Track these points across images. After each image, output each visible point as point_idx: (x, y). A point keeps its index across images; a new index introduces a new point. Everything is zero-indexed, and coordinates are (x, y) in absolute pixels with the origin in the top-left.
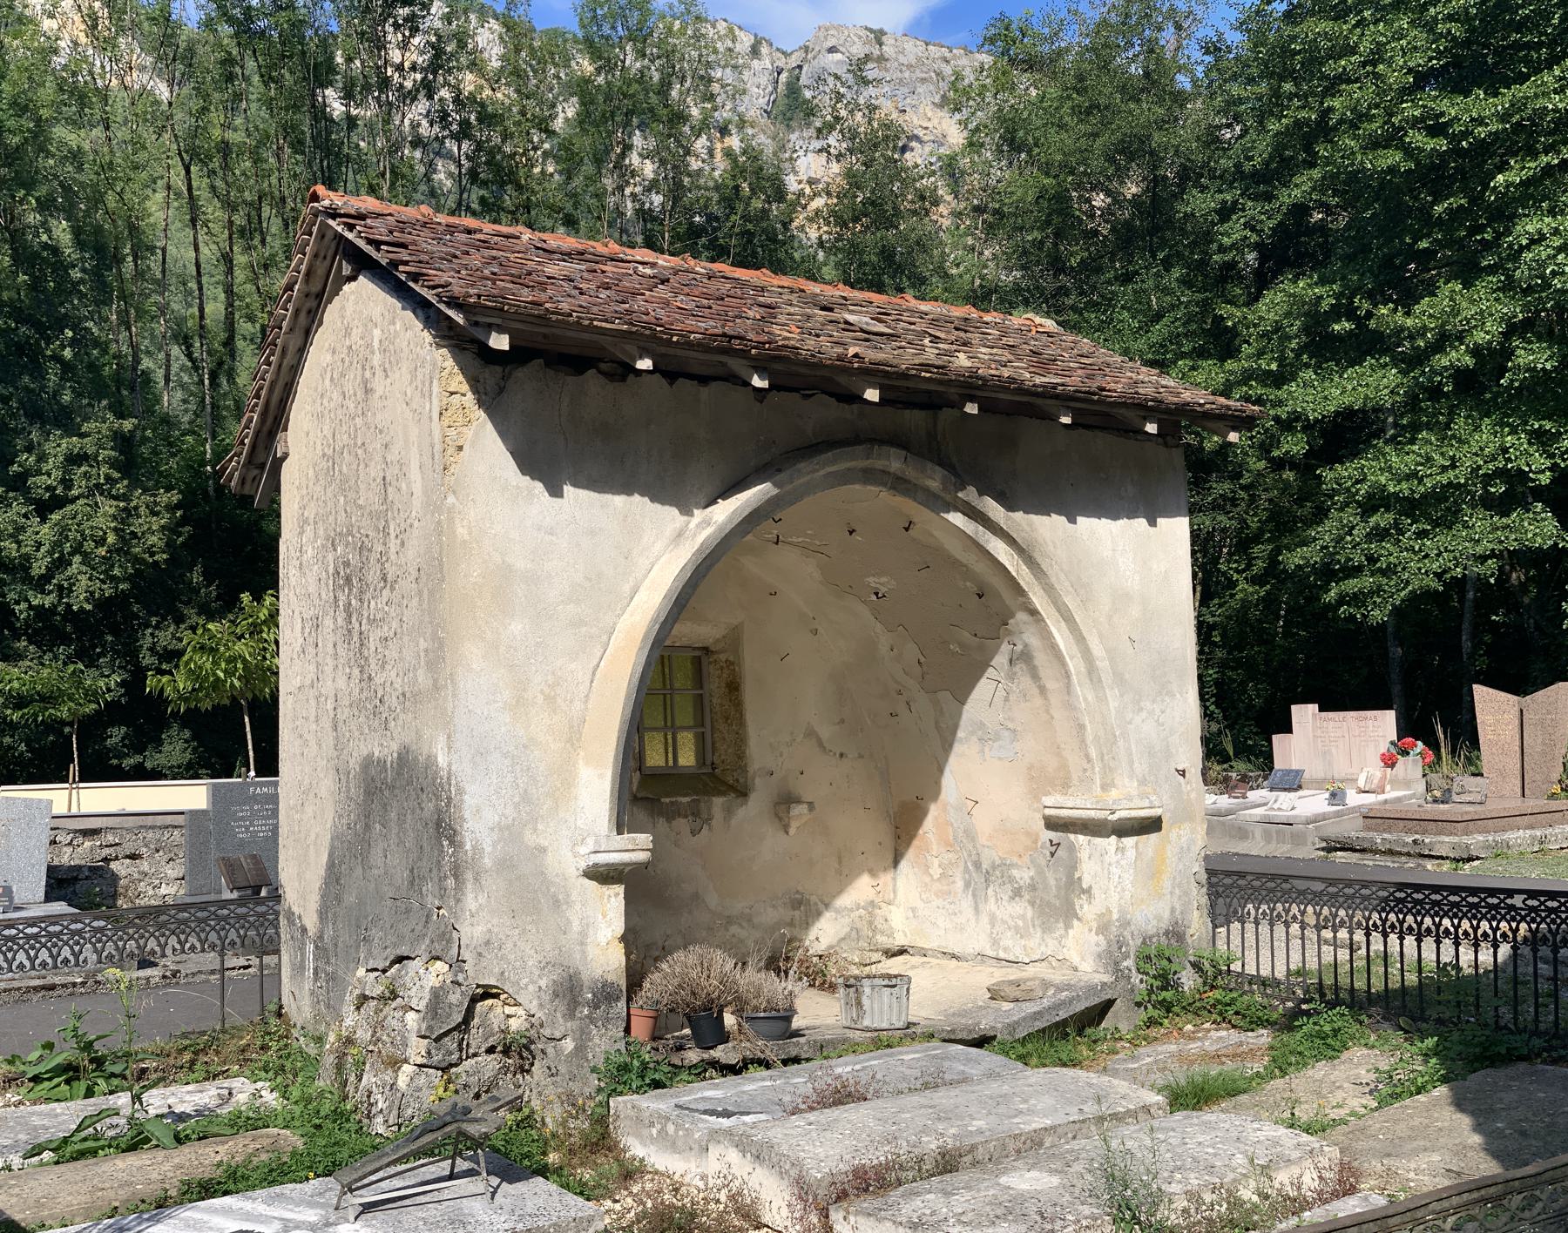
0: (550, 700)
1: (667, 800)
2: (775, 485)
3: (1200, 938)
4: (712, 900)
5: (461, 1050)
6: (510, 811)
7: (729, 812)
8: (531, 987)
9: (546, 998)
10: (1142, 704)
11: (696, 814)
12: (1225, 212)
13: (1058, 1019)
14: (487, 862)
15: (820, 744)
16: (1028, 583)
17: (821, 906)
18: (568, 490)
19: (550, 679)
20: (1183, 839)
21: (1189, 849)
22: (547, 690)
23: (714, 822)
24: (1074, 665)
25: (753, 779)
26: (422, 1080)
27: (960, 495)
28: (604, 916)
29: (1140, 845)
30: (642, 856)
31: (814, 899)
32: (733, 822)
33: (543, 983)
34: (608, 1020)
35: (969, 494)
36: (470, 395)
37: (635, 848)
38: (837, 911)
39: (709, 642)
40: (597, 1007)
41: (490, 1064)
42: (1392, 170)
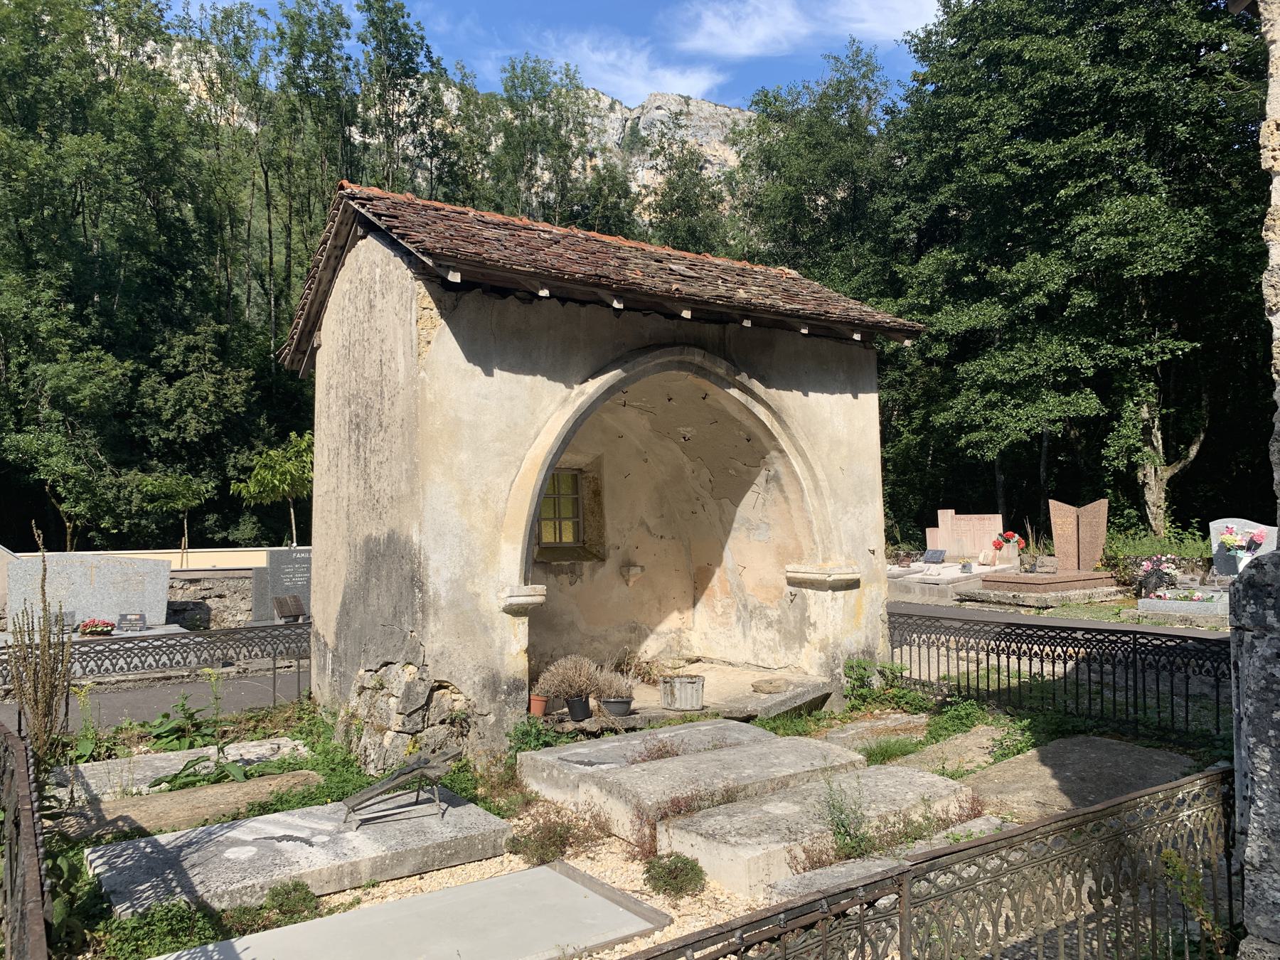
0: (484, 501)
4: (582, 626)
6: (458, 571)
7: (593, 571)
8: (469, 682)
9: (478, 688)
12: (898, 209)
14: (443, 603)
15: (649, 531)
17: (648, 631)
18: (496, 372)
19: (484, 489)
22: (482, 496)
24: (806, 484)
26: (399, 741)
28: (515, 637)
31: (644, 626)
32: (596, 577)
33: (476, 679)
35: (743, 377)
37: (535, 594)
40: (510, 694)
41: (442, 731)
42: (999, 185)
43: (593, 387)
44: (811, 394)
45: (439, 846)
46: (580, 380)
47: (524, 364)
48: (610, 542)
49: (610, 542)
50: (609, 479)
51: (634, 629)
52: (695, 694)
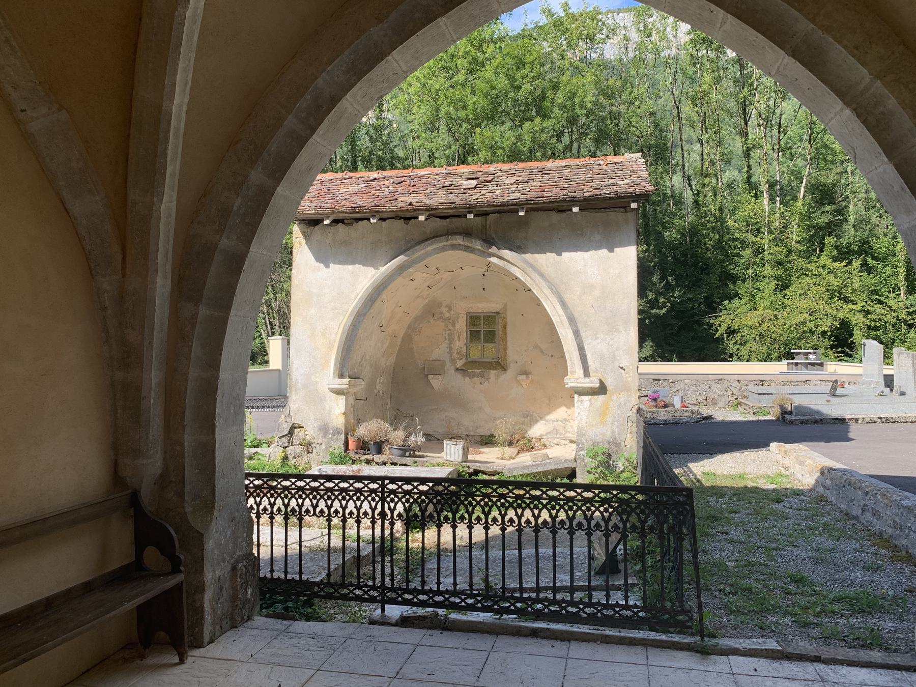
0: (323, 334)
2: (406, 256)
3: (631, 448)
5: (289, 443)
7: (498, 376)
8: (311, 426)
9: (316, 430)
10: (598, 336)
11: (483, 376)
14: (300, 385)
18: (332, 265)
20: (621, 400)
21: (625, 404)
23: (490, 380)
25: (510, 364)
26: (276, 450)
27: (490, 250)
28: (338, 405)
29: (592, 400)
30: (345, 386)
31: (534, 414)
33: (315, 425)
35: (494, 249)
36: (302, 237)
37: (344, 384)
38: (547, 421)
39: (498, 310)
40: (334, 435)
41: (299, 449)
43: (385, 269)
46: (383, 264)
47: (349, 259)
50: (511, 319)
52: (456, 452)
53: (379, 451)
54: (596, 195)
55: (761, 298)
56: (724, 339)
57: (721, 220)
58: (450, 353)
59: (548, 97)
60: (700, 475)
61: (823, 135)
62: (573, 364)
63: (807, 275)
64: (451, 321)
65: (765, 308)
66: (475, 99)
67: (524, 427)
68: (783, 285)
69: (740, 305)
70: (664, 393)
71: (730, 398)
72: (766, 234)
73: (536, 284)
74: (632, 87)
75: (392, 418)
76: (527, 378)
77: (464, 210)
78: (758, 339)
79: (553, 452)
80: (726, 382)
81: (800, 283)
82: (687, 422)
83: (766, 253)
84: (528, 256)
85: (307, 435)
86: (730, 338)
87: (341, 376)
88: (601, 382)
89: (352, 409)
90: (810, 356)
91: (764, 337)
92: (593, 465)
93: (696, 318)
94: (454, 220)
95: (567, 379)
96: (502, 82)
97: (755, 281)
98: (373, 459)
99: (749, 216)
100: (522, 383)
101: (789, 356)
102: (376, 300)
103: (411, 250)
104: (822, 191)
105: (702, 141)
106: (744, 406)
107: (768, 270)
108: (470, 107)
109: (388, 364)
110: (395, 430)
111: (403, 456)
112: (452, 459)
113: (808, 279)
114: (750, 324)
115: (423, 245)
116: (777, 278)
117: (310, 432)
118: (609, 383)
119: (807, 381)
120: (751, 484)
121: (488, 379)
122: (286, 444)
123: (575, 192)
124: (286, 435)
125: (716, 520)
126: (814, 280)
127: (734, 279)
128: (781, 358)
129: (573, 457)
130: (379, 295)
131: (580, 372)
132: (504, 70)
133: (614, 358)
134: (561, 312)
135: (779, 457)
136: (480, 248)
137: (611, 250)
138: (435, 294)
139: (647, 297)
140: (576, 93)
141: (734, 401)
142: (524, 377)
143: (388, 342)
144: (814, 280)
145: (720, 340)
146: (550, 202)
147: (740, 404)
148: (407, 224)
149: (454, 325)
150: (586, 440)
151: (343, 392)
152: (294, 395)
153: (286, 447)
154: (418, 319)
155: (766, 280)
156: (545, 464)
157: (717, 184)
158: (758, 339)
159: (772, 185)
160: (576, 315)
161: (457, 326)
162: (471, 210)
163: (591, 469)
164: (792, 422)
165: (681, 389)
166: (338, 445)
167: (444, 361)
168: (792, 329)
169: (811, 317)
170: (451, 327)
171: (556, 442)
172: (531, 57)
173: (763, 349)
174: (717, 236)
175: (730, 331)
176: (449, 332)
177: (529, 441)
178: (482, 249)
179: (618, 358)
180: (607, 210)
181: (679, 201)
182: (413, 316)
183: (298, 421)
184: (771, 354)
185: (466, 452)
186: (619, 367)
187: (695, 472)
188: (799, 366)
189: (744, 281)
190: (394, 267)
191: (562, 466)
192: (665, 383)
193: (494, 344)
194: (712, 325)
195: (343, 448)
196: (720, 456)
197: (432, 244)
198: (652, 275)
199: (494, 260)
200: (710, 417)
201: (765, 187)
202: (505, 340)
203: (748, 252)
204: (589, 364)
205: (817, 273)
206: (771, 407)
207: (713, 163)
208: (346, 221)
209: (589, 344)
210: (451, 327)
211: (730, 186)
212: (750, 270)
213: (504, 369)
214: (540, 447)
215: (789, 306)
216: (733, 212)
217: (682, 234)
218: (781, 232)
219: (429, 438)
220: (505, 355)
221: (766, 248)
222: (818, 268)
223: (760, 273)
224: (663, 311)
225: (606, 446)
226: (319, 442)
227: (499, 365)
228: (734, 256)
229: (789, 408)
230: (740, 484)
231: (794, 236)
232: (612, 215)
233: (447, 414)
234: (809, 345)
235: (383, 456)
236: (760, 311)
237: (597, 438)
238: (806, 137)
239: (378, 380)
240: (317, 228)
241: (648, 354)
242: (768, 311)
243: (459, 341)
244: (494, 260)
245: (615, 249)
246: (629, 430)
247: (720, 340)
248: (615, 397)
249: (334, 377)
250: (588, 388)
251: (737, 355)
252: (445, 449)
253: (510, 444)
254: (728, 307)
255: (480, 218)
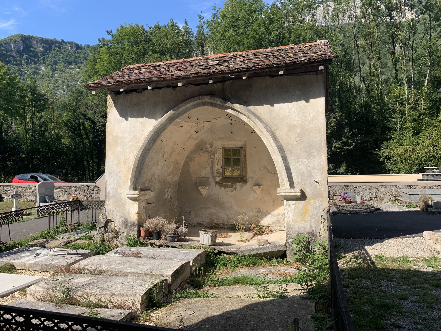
0: (125, 163)
1: (225, 183)
2: (173, 110)
3: (324, 237)
4: (236, 208)
5: (105, 231)
6: (115, 185)
7: (241, 187)
8: (118, 221)
9: (121, 223)
10: (299, 160)
11: (232, 187)
13: (260, 252)
14: (111, 195)
15: (268, 171)
16: (253, 126)
17: (267, 213)
18: (129, 119)
19: (125, 158)
20: (316, 204)
21: (319, 207)
22: (124, 160)
23: (237, 189)
26: (98, 236)
27: (226, 105)
28: (133, 208)
30: (137, 196)
31: (264, 211)
32: (242, 189)
33: (120, 220)
34: (134, 230)
35: (229, 104)
36: (112, 102)
37: (136, 194)
38: (272, 215)
39: (242, 145)
40: (131, 227)
44: (275, 105)
45: (45, 265)
48: (249, 176)
49: (249, 176)
50: (249, 151)
51: (259, 211)
53: (159, 237)
54: (295, 62)
55: (405, 140)
56: (385, 162)
57: (381, 98)
58: (212, 172)
59: (286, 37)
60: (374, 257)
61: (436, 52)
62: (282, 179)
63: (431, 127)
64: (212, 153)
65: (407, 145)
66: (248, 40)
67: (258, 219)
68: (417, 132)
69: (394, 143)
70: (350, 194)
71: (391, 196)
72: (407, 105)
73: (257, 126)
74: (331, 31)
75: (178, 213)
76: (259, 187)
77: (207, 77)
78: (404, 162)
79: (270, 238)
80: (388, 187)
81: (427, 131)
82: (364, 212)
83: (407, 115)
84: (251, 108)
85: (116, 226)
86: (388, 161)
87: (135, 189)
88: (302, 192)
89: (144, 210)
90: (435, 170)
91: (407, 160)
92: (298, 249)
93: (369, 151)
94: (203, 86)
95: (278, 190)
96: (262, 30)
97: (401, 130)
98: (154, 243)
99: (397, 96)
100: (256, 191)
101: (422, 170)
102: (156, 140)
103: (177, 107)
104: (437, 81)
105: (370, 58)
106: (400, 202)
107: (408, 124)
108: (246, 44)
109: (174, 180)
110: (168, 224)
111: (173, 241)
112: (204, 244)
113: (431, 129)
114: (399, 153)
115: (184, 103)
116: (414, 128)
117: (117, 224)
118: (308, 192)
119: (439, 186)
120: (413, 267)
121: (235, 189)
122: (104, 232)
123: (281, 61)
124: (103, 227)
125: (389, 309)
126: (435, 129)
127: (389, 130)
128: (417, 172)
129: (283, 243)
130: (158, 136)
131: (287, 185)
132: (263, 24)
133: (311, 175)
134: (273, 144)
135: (431, 243)
136: (220, 103)
137: (307, 101)
138: (202, 136)
139: (342, 140)
140: (301, 35)
141: (393, 198)
142: (257, 187)
143: (172, 167)
144: (435, 129)
145: (383, 162)
146: (263, 68)
147: (397, 200)
148: (175, 90)
149: (214, 155)
150: (293, 232)
151: (137, 199)
152: (108, 201)
153: (103, 234)
154: (193, 152)
155: (407, 130)
156: (265, 248)
157: (379, 80)
158: (404, 162)
159: (409, 79)
160: (284, 146)
161: (216, 156)
162: (211, 77)
163: (297, 252)
164: (433, 213)
165: (361, 192)
166: (133, 234)
167: (208, 178)
168: (423, 156)
169: (434, 149)
170: (212, 157)
171: (278, 229)
172: (277, 17)
173: (407, 167)
174: (380, 107)
175: (388, 157)
176: (211, 160)
177: (261, 228)
178: (221, 104)
179: (314, 175)
180: (304, 74)
181: (358, 90)
182: (189, 151)
183: (110, 218)
184: (411, 170)
185: (214, 238)
186: (315, 181)
187: (370, 254)
188: (429, 176)
189: (395, 131)
190: (166, 118)
191: (276, 250)
192: (351, 188)
193: (239, 167)
194: (378, 154)
195: (137, 236)
196: (387, 241)
197: (189, 102)
198: (345, 129)
199: (229, 111)
200: (379, 209)
201: (405, 81)
202: (245, 164)
203: (397, 115)
204: (294, 179)
205: (436, 125)
206: (417, 202)
207: (376, 69)
208: (138, 90)
209: (294, 166)
210: (212, 157)
211: (386, 81)
212: (398, 124)
213: (245, 182)
214: (268, 232)
215: (421, 143)
216: (388, 94)
217: (361, 108)
218: (415, 104)
219: (200, 225)
220: (246, 173)
221: (407, 112)
222: (437, 122)
223: (404, 126)
224: (351, 147)
225: (307, 236)
226: (123, 231)
227: (242, 179)
228: (389, 118)
229: (430, 203)
230: (404, 267)
231: (423, 105)
232: (307, 77)
233: (211, 210)
234: (433, 164)
235: (161, 241)
236: (405, 147)
237: (301, 230)
238: (427, 54)
239: (166, 191)
240: (120, 96)
241: (343, 171)
242: (409, 146)
243: (217, 165)
244: (229, 111)
245: (310, 100)
246: (322, 225)
247: (383, 162)
248: (312, 202)
249: (130, 190)
250: (293, 196)
251: (392, 170)
252: (200, 237)
253: (248, 230)
254: (386, 144)
255: (220, 84)
